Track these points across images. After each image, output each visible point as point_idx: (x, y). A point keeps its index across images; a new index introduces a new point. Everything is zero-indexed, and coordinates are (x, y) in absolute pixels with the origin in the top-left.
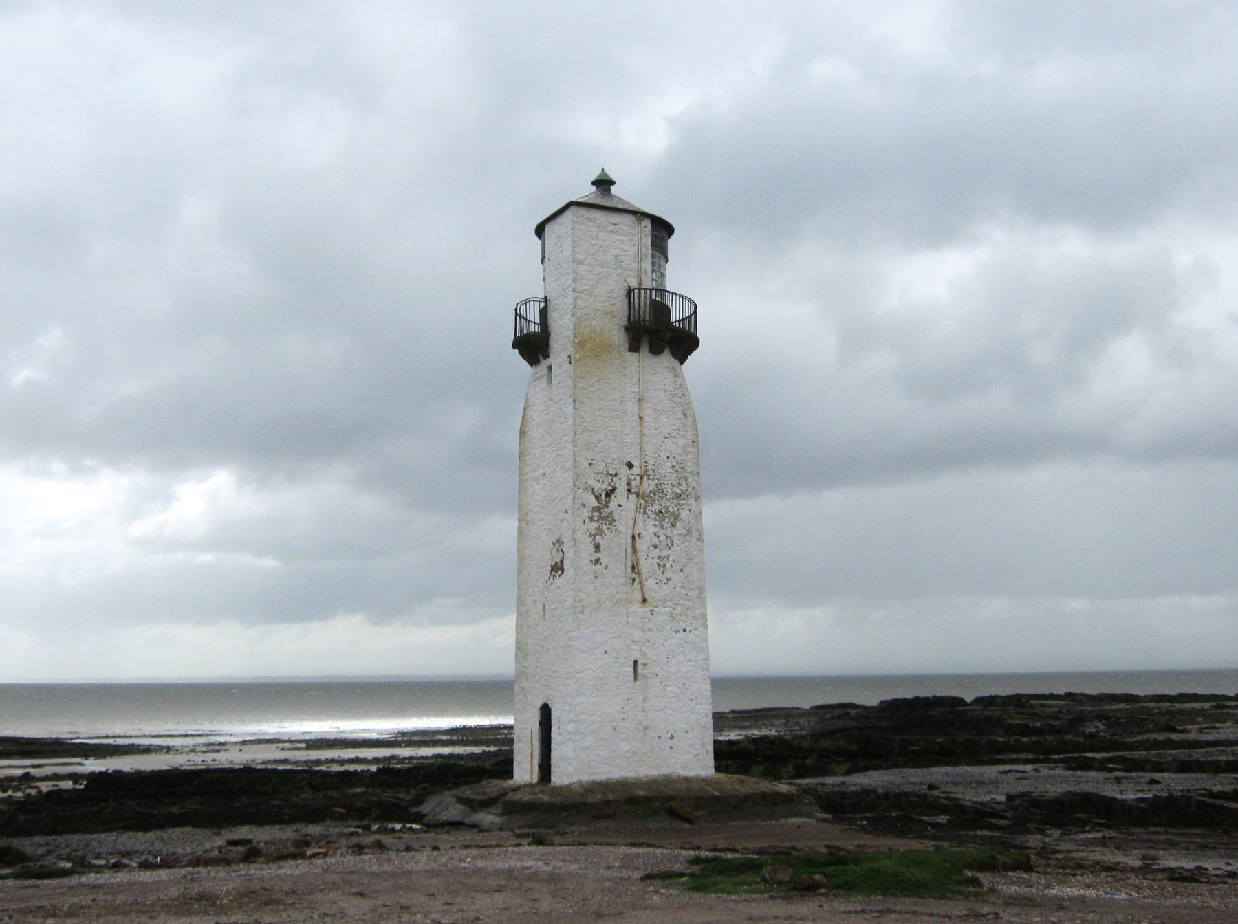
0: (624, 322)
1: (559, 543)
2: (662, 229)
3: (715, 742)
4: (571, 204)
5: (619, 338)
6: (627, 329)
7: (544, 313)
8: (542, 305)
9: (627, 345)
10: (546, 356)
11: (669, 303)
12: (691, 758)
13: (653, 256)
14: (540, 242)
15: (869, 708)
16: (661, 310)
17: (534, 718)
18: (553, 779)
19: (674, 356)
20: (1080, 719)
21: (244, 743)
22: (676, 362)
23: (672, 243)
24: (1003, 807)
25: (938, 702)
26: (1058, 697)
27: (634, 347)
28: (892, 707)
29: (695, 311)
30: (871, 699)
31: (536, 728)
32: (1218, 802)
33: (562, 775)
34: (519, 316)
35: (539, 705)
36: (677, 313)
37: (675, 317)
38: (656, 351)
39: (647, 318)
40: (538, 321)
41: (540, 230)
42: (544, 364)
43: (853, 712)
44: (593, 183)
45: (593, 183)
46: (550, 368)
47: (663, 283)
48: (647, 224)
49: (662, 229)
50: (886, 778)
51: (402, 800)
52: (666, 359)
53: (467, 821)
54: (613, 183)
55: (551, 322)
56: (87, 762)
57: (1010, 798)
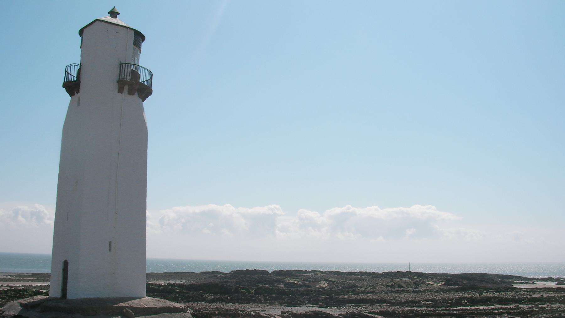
2: (139, 37)
3: (148, 285)
4: (97, 20)
5: (114, 86)
6: (118, 82)
7: (79, 72)
8: (79, 67)
10: (78, 92)
11: (139, 72)
13: (134, 49)
15: (224, 274)
16: (135, 75)
17: (61, 267)
19: (139, 97)
20: (317, 280)
23: (144, 45)
26: (309, 272)
27: (120, 91)
29: (151, 78)
30: (227, 271)
31: (61, 271)
32: (373, 316)
33: (69, 296)
34: (67, 73)
35: (63, 261)
36: (143, 77)
37: (141, 80)
38: (131, 93)
40: (75, 75)
41: (81, 32)
42: (77, 95)
43: (218, 275)
44: (109, 13)
45: (109, 13)
46: (79, 98)
48: (133, 33)
49: (139, 37)
50: (311, 309)
52: (136, 97)
54: (119, 14)
57: (347, 313)
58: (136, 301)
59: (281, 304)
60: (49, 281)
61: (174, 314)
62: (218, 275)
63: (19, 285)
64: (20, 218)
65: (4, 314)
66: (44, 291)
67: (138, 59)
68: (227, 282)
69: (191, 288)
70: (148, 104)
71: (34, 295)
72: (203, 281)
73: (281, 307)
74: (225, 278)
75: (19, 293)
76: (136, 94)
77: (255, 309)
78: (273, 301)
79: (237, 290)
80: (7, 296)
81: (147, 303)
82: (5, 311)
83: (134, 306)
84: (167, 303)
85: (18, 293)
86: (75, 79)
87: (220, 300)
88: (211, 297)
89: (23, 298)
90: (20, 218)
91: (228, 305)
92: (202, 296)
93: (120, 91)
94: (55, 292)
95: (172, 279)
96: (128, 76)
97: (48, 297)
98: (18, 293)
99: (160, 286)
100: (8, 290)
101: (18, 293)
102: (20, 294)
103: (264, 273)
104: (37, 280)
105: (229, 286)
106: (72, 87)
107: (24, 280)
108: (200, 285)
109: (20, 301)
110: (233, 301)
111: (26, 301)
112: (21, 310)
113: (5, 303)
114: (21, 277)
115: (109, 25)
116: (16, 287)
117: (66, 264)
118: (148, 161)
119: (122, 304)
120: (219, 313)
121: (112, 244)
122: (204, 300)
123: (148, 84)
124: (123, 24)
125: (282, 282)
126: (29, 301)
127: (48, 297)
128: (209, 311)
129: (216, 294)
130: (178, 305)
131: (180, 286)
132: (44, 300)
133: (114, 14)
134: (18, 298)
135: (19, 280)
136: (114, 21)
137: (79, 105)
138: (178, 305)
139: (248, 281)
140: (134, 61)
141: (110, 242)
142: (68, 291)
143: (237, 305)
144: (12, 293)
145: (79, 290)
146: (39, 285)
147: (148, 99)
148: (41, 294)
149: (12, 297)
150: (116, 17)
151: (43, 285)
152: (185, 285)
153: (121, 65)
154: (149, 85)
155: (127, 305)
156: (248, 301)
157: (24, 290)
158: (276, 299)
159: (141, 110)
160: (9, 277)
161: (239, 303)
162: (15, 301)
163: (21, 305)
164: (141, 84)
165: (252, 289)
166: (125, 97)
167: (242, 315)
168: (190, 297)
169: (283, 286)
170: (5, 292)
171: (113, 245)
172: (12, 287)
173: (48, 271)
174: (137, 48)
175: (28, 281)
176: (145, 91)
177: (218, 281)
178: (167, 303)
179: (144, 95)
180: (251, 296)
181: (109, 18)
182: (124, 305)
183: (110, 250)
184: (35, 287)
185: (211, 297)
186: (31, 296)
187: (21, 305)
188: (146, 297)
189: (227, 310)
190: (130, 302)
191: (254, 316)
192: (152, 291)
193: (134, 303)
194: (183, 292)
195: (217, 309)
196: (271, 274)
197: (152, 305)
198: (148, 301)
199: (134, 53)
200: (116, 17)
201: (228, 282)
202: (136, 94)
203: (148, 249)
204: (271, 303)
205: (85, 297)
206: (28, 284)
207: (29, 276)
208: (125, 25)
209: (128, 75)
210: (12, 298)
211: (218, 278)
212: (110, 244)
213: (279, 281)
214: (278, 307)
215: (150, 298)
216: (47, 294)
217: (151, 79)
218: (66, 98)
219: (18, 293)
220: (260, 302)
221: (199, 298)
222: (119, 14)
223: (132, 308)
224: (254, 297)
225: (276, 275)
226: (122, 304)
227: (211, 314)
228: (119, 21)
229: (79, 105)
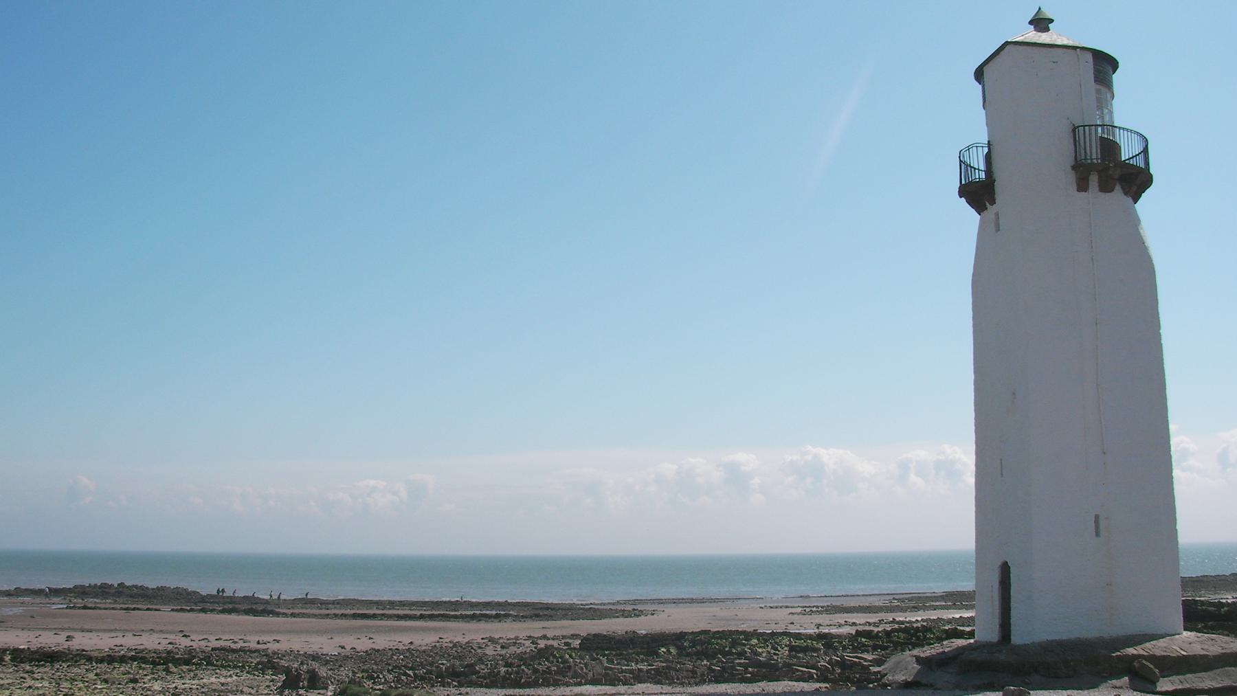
0: (1071, 161)
2: (1104, 64)
3: (1185, 604)
4: (1007, 43)
6: (1074, 168)
7: (988, 158)
8: (986, 150)
9: (1075, 187)
10: (993, 202)
12: (215, 593)
13: (1098, 92)
16: (1110, 148)
17: (995, 577)
18: (1013, 638)
19: (1126, 193)
20: (1205, 627)
21: (81, 592)
22: (1130, 200)
23: (1117, 78)
27: (1082, 186)
31: (996, 585)
33: (1017, 638)
34: (964, 166)
36: (1128, 150)
38: (1105, 187)
40: (982, 167)
41: (979, 75)
42: (992, 210)
44: (1031, 23)
45: (1031, 23)
46: (997, 215)
47: (1107, 119)
48: (1089, 56)
49: (1104, 64)
51: (865, 660)
52: (1117, 195)
54: (1051, 21)
55: (995, 168)
58: (1162, 643)
60: (971, 607)
63: (916, 617)
64: (913, 478)
65: (885, 680)
66: (968, 629)
67: (1111, 113)
70: (1146, 206)
71: (946, 639)
75: (915, 636)
76: (1118, 188)
80: (892, 642)
81: (1185, 646)
83: (1158, 653)
84: (1232, 645)
86: (983, 175)
89: (923, 646)
90: (913, 478)
93: (1082, 186)
94: (987, 632)
96: (1094, 154)
98: (915, 635)
99: (1221, 605)
100: (893, 631)
101: (912, 635)
102: (918, 638)
104: (954, 607)
106: (978, 193)
107: (925, 608)
109: (916, 652)
111: (927, 652)
112: (919, 672)
113: (887, 657)
114: (919, 602)
115: (1036, 49)
116: (910, 622)
117: (1005, 569)
118: (1165, 332)
119: (1131, 651)
124: (1066, 42)
126: (933, 652)
132: (963, 648)
133: (1041, 23)
134: (915, 646)
135: (916, 609)
136: (1044, 38)
140: (1102, 118)
141: (1097, 517)
142: (1013, 628)
144: (902, 635)
145: (1036, 625)
146: (957, 616)
148: (961, 635)
150: (1047, 30)
153: (1074, 130)
154: (1142, 165)
155: (1142, 652)
157: (926, 629)
159: (1135, 221)
160: (896, 603)
162: (908, 652)
163: (919, 660)
164: (1125, 165)
170: (888, 634)
171: (1102, 523)
172: (902, 623)
173: (968, 585)
174: (1104, 89)
175: (943, 608)
176: (1136, 180)
178: (1232, 645)
179: (1135, 188)
181: (1032, 35)
183: (1097, 534)
184: (949, 621)
186: (940, 640)
187: (919, 660)
188: (1185, 633)
190: (1148, 645)
192: (1198, 616)
193: (1157, 647)
197: (1197, 650)
198: (1188, 642)
199: (1098, 100)
200: (1047, 30)
202: (1118, 188)
203: (1180, 526)
205: (1051, 638)
206: (933, 615)
207: (936, 598)
208: (1070, 43)
210: (901, 646)
216: (971, 634)
217: (1145, 151)
218: (970, 218)
219: (912, 635)
222: (1051, 21)
223: (1152, 658)
226: (1131, 651)
228: (1055, 37)
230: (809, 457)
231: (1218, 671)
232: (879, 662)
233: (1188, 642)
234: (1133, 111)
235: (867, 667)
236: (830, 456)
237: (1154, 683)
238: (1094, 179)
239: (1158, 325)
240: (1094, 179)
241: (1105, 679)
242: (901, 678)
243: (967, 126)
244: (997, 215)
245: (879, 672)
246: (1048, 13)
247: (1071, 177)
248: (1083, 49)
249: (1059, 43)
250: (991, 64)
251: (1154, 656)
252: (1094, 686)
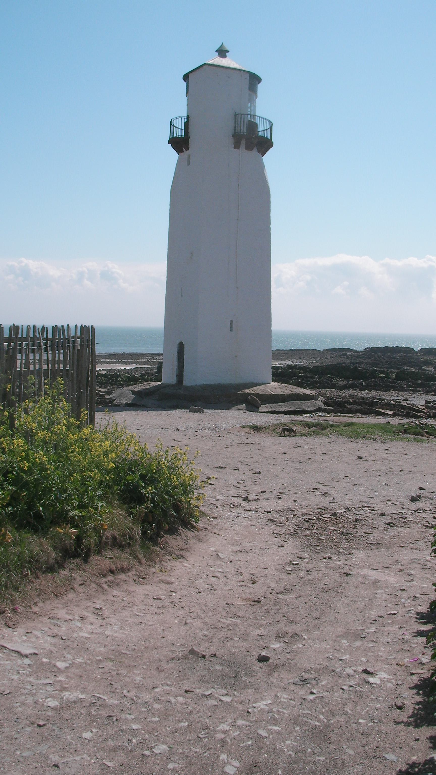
1: (298, 557)
2: (254, 79)
4: (205, 64)
6: (233, 136)
7: (187, 124)
10: (187, 149)
11: (257, 122)
14: (186, 83)
15: (355, 351)
16: (252, 126)
19: (259, 152)
22: (260, 155)
23: (260, 87)
24: (423, 407)
25: (398, 349)
27: (237, 146)
28: (373, 352)
33: (187, 382)
34: (173, 127)
35: (178, 342)
36: (261, 127)
37: (260, 128)
38: (249, 147)
39: (245, 131)
40: (183, 128)
41: (186, 78)
42: (186, 153)
43: (349, 354)
44: (216, 51)
45: (216, 51)
46: (189, 157)
47: (255, 113)
48: (247, 76)
49: (254, 79)
52: (255, 152)
53: (139, 404)
54: (228, 51)
56: (309, 393)
58: (262, 387)
59: (427, 393)
61: (304, 402)
62: (349, 354)
64: (87, 282)
68: (360, 363)
69: (317, 371)
70: (269, 158)
72: (327, 361)
73: (427, 397)
74: (358, 357)
76: (255, 148)
77: (395, 398)
78: (418, 389)
79: (373, 375)
81: (273, 390)
82: (115, 400)
83: (260, 393)
85: (111, 378)
87: (353, 387)
88: (342, 383)
90: (87, 282)
91: (363, 392)
92: (331, 381)
93: (237, 146)
95: (288, 359)
96: (244, 129)
97: (160, 383)
98: (111, 378)
102: (113, 380)
103: (409, 350)
104: (117, 362)
105: (364, 369)
106: (179, 144)
108: (327, 367)
109: (130, 388)
110: (369, 388)
111: (138, 388)
113: (114, 390)
117: (181, 346)
119: (247, 391)
120: (354, 402)
121: (234, 322)
122: (333, 386)
123: (267, 136)
125: (432, 364)
127: (160, 383)
128: (343, 398)
129: (347, 378)
130: (308, 392)
131: (302, 368)
132: (156, 386)
137: (189, 164)
138: (308, 392)
139: (387, 362)
143: (373, 392)
146: (123, 368)
147: (269, 153)
149: (105, 384)
151: (128, 368)
152: (309, 368)
153: (235, 115)
154: (269, 137)
156: (387, 388)
158: (421, 386)
159: (261, 167)
161: (377, 390)
162: (125, 388)
163: (133, 392)
165: (393, 373)
166: (242, 152)
167: (380, 404)
168: (317, 382)
169: (432, 369)
175: (107, 363)
176: (265, 145)
177: (349, 361)
178: (295, 390)
180: (390, 382)
182: (249, 392)
185: (342, 383)
187: (133, 392)
189: (363, 398)
190: (255, 388)
191: (394, 405)
192: (279, 375)
193: (260, 390)
194: (307, 377)
195: (351, 396)
196: (417, 352)
198: (274, 388)
201: (362, 363)
202: (255, 148)
204: (415, 391)
209: (245, 127)
211: (348, 358)
212: (231, 324)
213: (427, 363)
214: (424, 396)
215: (276, 383)
217: (271, 128)
218: (173, 156)
220: (401, 389)
221: (329, 384)
222: (228, 51)
223: (257, 395)
224: (394, 383)
225: (424, 355)
226: (247, 391)
227: (345, 402)
229: (189, 164)
230: (23, 264)
231: (288, 403)
232: (109, 393)
233: (274, 388)
234: (266, 108)
235: (103, 396)
236: (33, 265)
237: (258, 408)
238: (243, 143)
239: (270, 224)
240: (243, 143)
241: (234, 405)
242: (124, 401)
243: (177, 107)
244: (189, 157)
245: (111, 398)
246: (227, 47)
247: (231, 141)
248: (244, 71)
249: (232, 66)
250: (193, 73)
251: (258, 394)
252: (228, 408)
